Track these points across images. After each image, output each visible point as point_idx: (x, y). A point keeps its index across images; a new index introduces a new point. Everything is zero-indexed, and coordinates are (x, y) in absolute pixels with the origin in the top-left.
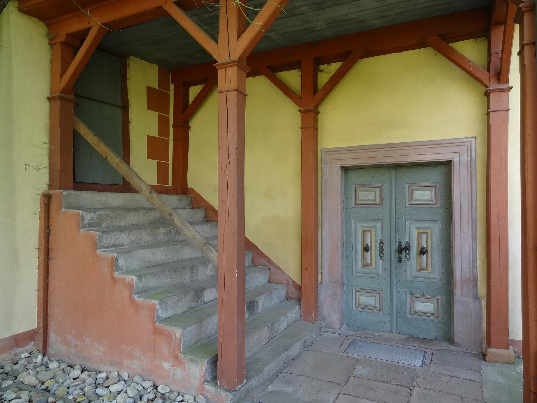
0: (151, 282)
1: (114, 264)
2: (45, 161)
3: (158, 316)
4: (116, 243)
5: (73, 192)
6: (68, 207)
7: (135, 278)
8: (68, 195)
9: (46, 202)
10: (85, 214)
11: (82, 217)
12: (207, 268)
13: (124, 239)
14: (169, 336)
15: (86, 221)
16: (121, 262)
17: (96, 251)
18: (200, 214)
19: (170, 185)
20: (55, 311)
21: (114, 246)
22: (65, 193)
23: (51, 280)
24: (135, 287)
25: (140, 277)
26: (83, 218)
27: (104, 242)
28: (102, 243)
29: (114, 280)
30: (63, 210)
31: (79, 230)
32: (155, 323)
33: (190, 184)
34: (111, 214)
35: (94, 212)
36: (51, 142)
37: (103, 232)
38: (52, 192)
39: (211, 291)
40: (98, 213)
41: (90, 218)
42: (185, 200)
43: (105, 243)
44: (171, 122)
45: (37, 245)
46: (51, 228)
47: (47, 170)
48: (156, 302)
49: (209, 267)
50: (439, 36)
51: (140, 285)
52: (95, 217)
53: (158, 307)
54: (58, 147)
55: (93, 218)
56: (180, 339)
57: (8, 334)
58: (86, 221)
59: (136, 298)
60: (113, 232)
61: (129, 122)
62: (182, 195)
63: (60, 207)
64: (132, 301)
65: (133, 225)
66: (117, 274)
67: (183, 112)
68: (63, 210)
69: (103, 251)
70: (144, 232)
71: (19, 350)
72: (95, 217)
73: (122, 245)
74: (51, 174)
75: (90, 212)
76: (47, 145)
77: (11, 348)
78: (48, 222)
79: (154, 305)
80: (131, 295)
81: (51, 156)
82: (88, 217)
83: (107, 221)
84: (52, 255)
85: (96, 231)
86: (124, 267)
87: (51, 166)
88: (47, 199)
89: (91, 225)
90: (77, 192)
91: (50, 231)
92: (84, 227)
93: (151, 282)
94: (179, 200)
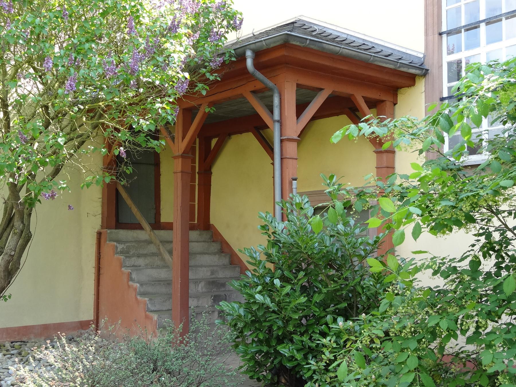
0: (150, 289)
1: (130, 278)
2: (99, 210)
3: (148, 308)
4: (135, 264)
5: (114, 230)
6: (110, 241)
7: (138, 285)
8: (111, 232)
9: (98, 237)
10: (118, 245)
11: (116, 247)
12: (198, 286)
13: (141, 262)
14: (151, 319)
15: (119, 250)
16: (134, 276)
17: (121, 268)
18: (215, 247)
19: (196, 222)
20: (102, 308)
21: (133, 266)
22: (109, 231)
23: (100, 288)
24: (138, 290)
25: (142, 285)
26: (117, 247)
27: (127, 263)
28: (126, 264)
29: (129, 286)
30: (108, 242)
31: (114, 255)
32: (146, 312)
33: (212, 222)
34: (136, 245)
35: (124, 244)
36: (103, 198)
37: (126, 257)
38: (102, 231)
39: (193, 300)
40: (127, 244)
41: (121, 248)
42: (206, 235)
43: (127, 264)
44: (197, 170)
45: (94, 265)
46: (101, 254)
47: (100, 216)
48: (147, 299)
49: (200, 285)
50: (349, 108)
51: (142, 290)
52: (125, 247)
53: (148, 302)
54: (106, 201)
55: (123, 247)
56: (156, 321)
57: (77, 320)
58: (119, 250)
59: (139, 297)
60: (133, 257)
61: (160, 175)
62: (204, 230)
63: (106, 241)
64: (136, 298)
65: (152, 253)
66: (131, 283)
67: (204, 162)
68: (108, 242)
69: (125, 269)
70: (156, 258)
71: (83, 331)
72: (125, 247)
73: (140, 266)
74: (102, 218)
75: (121, 244)
76: (101, 200)
77: (78, 329)
78: (100, 250)
79: (145, 301)
80: (136, 295)
81: (103, 208)
82: (120, 247)
83: (133, 250)
84: (102, 271)
85: (122, 256)
86: (136, 279)
87: (103, 214)
88: (99, 234)
89: (122, 252)
90: (117, 230)
91: (100, 256)
92: (118, 253)
93: (150, 289)
94: (200, 235)
